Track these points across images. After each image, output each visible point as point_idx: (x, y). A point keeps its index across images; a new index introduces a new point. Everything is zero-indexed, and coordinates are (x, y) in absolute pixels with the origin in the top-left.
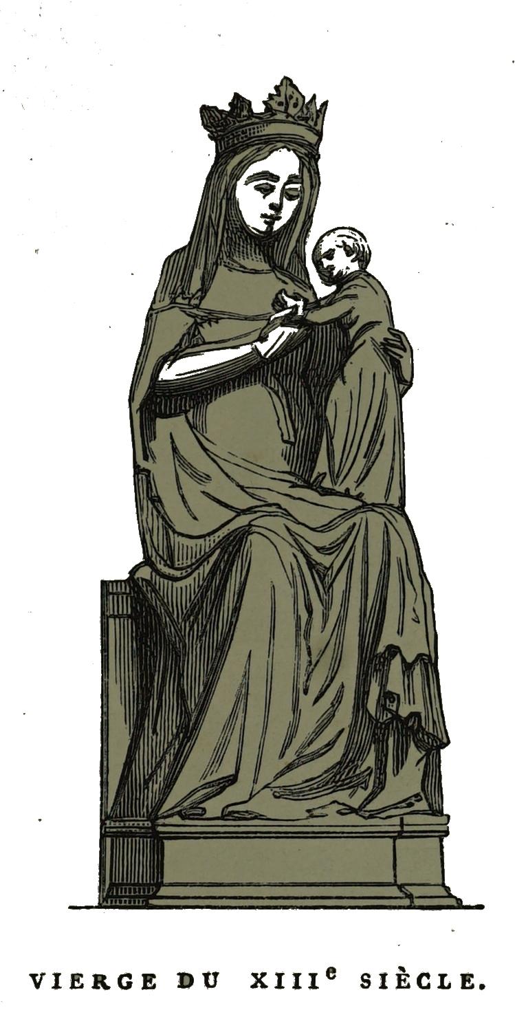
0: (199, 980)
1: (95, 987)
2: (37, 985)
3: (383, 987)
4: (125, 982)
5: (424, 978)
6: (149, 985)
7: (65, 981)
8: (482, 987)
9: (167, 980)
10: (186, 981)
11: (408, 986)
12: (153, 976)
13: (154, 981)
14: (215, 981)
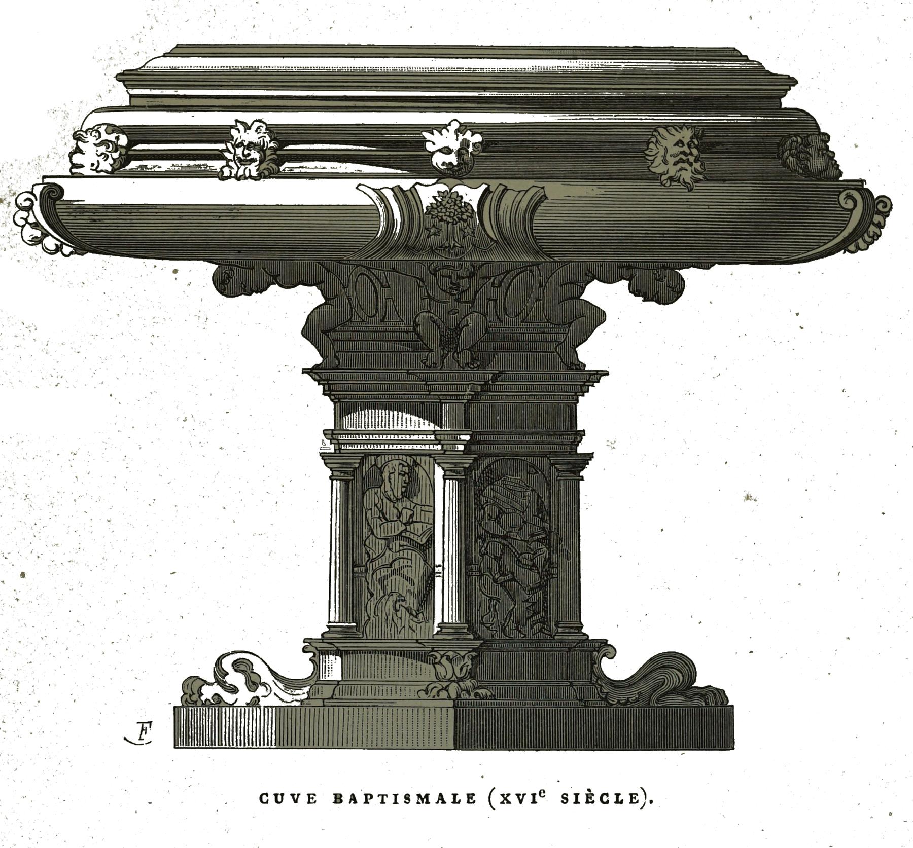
2: (521, 802)
3: (577, 802)
5: (605, 797)
9: (325, 799)
11: (593, 802)
12: (473, 795)
13: (474, 798)
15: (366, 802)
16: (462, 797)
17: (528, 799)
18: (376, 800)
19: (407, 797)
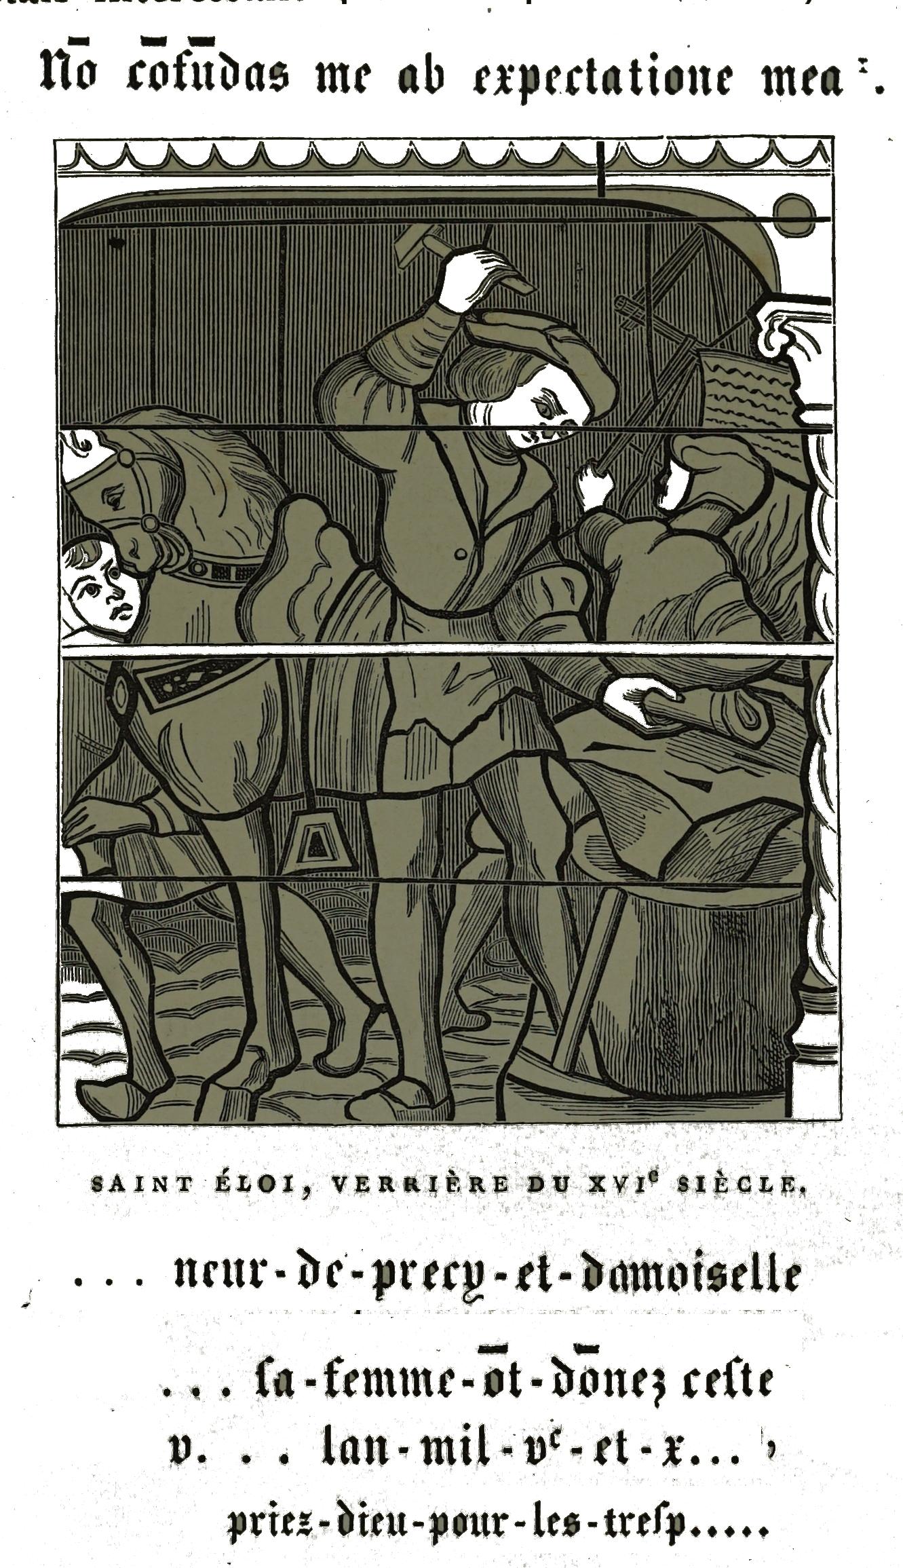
0: (549, 1184)
1: (382, 1190)
2: (340, 1188)
4: (743, 1184)
5: (745, 1181)
6: (362, 1187)
7: (148, 1184)
8: (803, 1190)
10: (597, 1184)
14: (566, 1186)
15: (184, 1189)
16: (775, 1182)
17: (632, 1184)
18: (253, 1180)
19: (452, 1181)
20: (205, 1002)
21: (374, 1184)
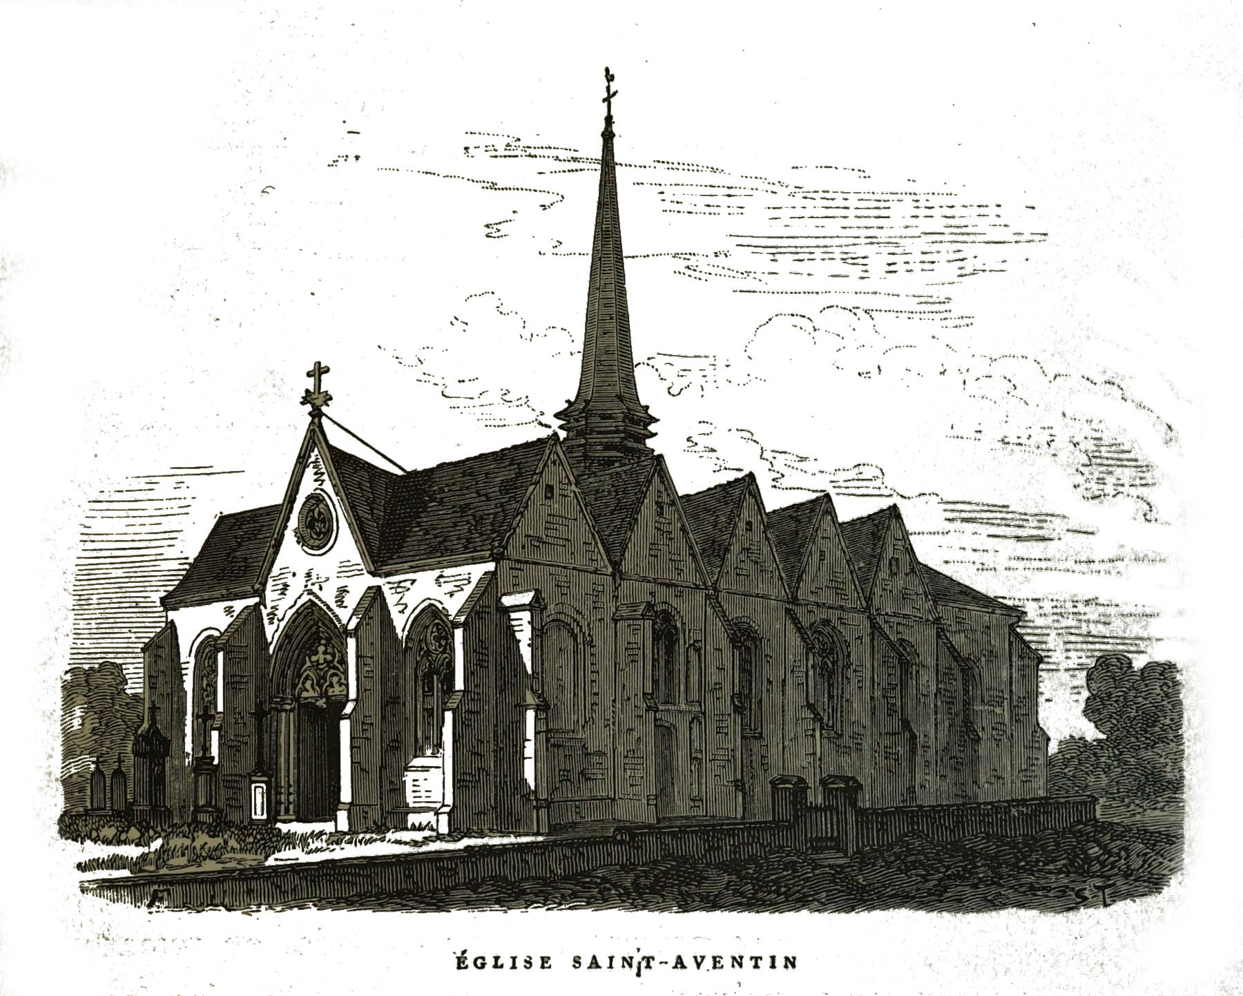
2: (698, 965)
3: (514, 967)
7: (780, 962)
9: (561, 962)
20: (66, 832)
21: (727, 962)
